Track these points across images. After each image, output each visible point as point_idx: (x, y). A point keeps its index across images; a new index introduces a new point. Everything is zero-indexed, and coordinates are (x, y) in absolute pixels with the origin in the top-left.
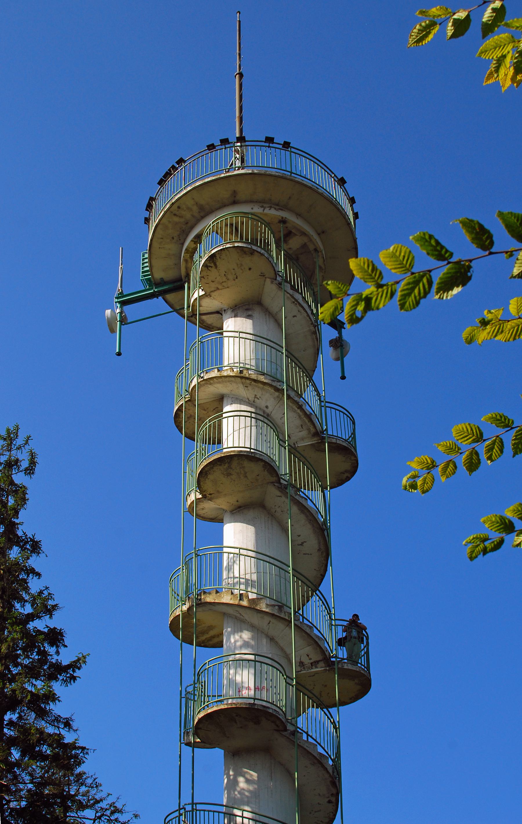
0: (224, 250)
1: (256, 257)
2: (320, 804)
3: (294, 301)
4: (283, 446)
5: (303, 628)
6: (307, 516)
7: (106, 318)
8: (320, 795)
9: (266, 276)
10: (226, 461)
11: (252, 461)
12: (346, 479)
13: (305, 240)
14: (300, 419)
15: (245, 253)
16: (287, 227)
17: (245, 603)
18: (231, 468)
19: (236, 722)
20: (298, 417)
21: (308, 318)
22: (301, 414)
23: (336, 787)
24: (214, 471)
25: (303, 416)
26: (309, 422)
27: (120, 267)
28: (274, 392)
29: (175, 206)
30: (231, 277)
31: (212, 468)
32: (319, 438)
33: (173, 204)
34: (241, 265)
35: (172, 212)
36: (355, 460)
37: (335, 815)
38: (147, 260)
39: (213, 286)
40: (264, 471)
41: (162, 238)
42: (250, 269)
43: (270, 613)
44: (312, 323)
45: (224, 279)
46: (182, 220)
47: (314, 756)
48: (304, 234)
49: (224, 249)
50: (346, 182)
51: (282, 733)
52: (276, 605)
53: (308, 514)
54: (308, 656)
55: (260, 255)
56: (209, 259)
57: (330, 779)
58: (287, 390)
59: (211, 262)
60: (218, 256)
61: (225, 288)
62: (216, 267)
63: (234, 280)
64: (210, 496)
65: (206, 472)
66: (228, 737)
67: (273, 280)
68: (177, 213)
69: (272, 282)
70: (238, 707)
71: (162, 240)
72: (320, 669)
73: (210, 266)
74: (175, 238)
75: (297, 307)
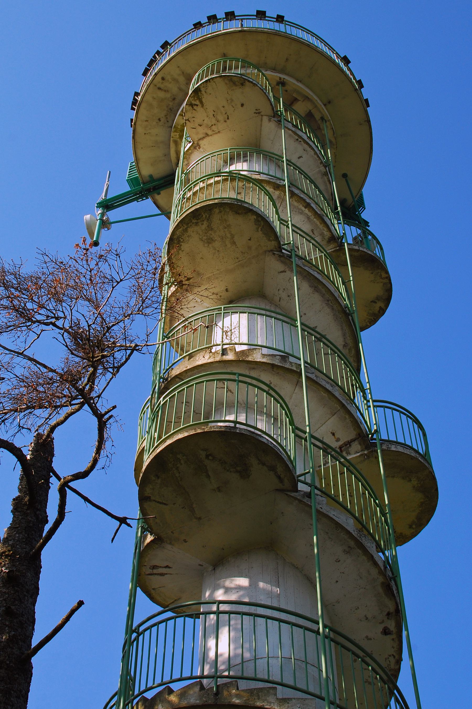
0: (210, 82)
1: (248, 89)
2: (370, 639)
3: (297, 138)
4: (284, 225)
5: (321, 383)
6: (323, 295)
7: (85, 220)
8: (367, 619)
9: (262, 114)
10: (204, 216)
11: (239, 214)
12: (379, 312)
13: (309, 106)
14: (310, 221)
15: (234, 83)
16: (286, 91)
17: (230, 357)
18: (212, 229)
19: (208, 476)
20: (306, 220)
21: (316, 156)
22: (310, 214)
23: (393, 595)
24: (188, 236)
25: (313, 217)
26: (321, 224)
27: (106, 183)
28: (274, 191)
29: (159, 77)
30: (221, 118)
31: (186, 230)
32: (336, 244)
33: (156, 74)
34: (232, 100)
35: (156, 86)
36: (387, 278)
37: (399, 661)
38: (134, 164)
39: (202, 131)
40: (258, 231)
41: (147, 121)
42: (242, 105)
43: (268, 364)
44: (321, 163)
45: (214, 121)
46: (168, 95)
47: (348, 533)
48: (307, 98)
49: (209, 80)
50: (350, 62)
51: (289, 493)
52: (278, 355)
53: (323, 290)
54: (333, 434)
55: (252, 84)
56: (193, 94)
57: (381, 579)
58: (289, 187)
59: (196, 98)
60: (203, 89)
61: (216, 133)
62: (203, 106)
63: (225, 121)
64: (187, 282)
65: (178, 238)
66: (200, 518)
67: (271, 117)
68: (162, 86)
69: (270, 120)
70: (206, 432)
71: (147, 123)
72: (355, 456)
73: (195, 105)
74: (162, 119)
75: (301, 144)
